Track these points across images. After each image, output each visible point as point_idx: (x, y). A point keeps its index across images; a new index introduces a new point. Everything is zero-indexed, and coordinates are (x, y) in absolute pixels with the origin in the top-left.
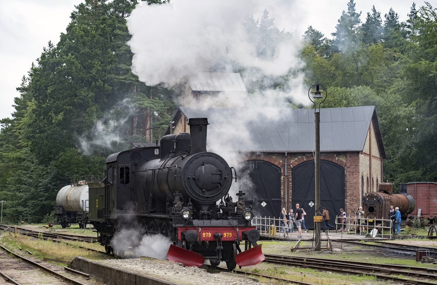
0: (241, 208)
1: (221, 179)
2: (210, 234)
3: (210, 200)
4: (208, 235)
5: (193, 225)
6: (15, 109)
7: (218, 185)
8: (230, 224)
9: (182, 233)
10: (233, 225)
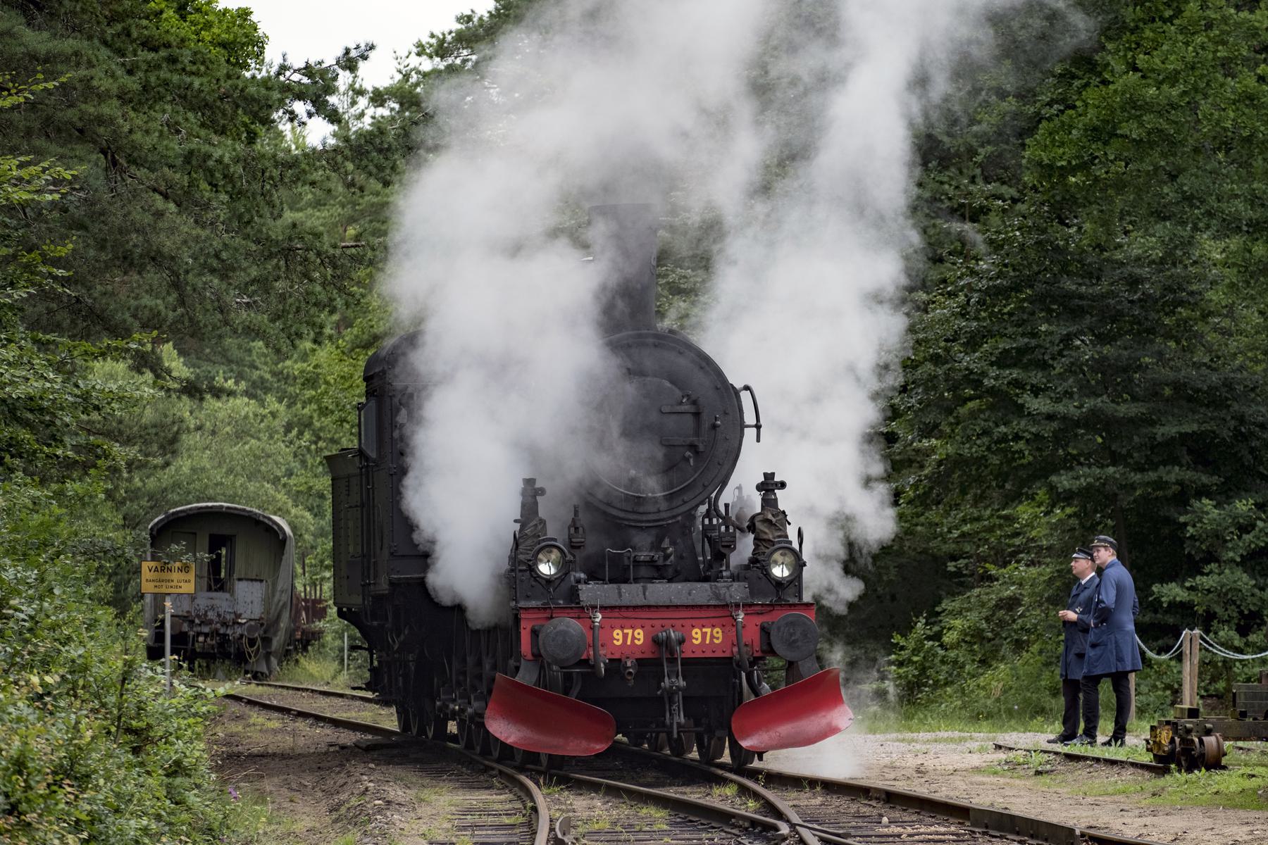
0: (771, 537)
1: (697, 432)
2: (640, 635)
3: (685, 502)
4: (633, 638)
5: (578, 603)
6: (330, 125)
7: (688, 454)
8: (717, 596)
9: (535, 633)
10: (728, 600)
